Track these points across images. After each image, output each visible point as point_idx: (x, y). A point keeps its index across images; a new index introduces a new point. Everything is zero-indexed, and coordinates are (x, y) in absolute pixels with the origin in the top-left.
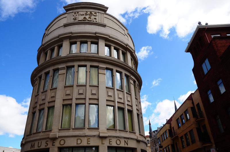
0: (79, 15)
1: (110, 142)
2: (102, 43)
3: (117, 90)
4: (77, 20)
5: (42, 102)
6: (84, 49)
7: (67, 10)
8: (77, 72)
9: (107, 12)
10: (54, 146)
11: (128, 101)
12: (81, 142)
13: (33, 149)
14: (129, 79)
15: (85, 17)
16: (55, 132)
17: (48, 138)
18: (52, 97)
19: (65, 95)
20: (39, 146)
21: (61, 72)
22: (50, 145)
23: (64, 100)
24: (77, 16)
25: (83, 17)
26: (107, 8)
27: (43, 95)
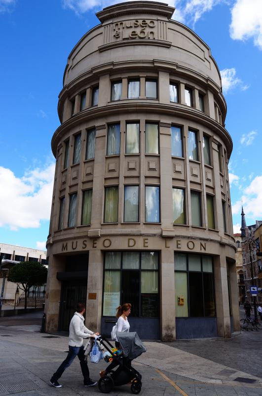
0: (124, 28)
1: (178, 244)
2: (164, 79)
3: (190, 161)
5: (73, 183)
10: (95, 249)
11: (208, 180)
12: (135, 244)
13: (65, 251)
15: (134, 32)
16: (95, 228)
17: (86, 236)
18: (88, 175)
21: (99, 133)
22: (89, 247)
23: (106, 179)
24: (121, 31)
25: (130, 31)
27: (74, 171)
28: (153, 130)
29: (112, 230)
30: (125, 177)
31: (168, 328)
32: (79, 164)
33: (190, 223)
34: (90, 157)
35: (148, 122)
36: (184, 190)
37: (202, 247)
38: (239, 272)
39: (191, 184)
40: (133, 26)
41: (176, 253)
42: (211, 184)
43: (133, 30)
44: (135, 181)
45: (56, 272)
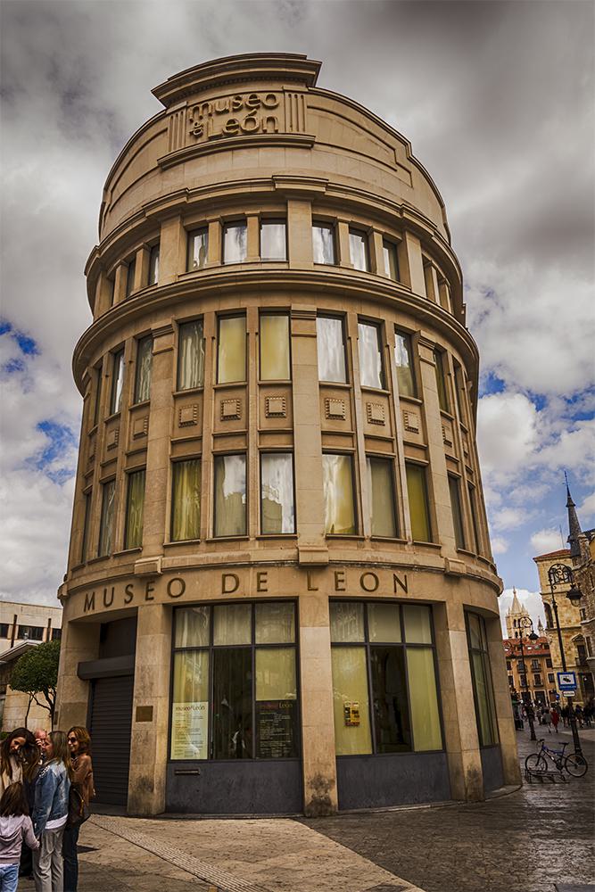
0: (210, 115)
1: (337, 581)
2: (299, 215)
3: (364, 391)
4: (204, 138)
5: (108, 457)
6: (236, 250)
7: (168, 102)
8: (257, 334)
9: (322, 83)
10: (152, 602)
11: (410, 429)
13: (90, 612)
14: (414, 343)
15: (232, 121)
16: (153, 556)
17: (132, 576)
18: (137, 436)
19: (176, 426)
20: (108, 602)
21: (159, 343)
22: (138, 600)
23: (174, 444)
24: (203, 122)
26: (316, 67)
27: (111, 432)
28: (277, 330)
29: (187, 557)
30: (216, 437)
31: (319, 783)
32: (119, 416)
33: (368, 532)
34: (143, 397)
35: (263, 312)
36: (350, 456)
37: (398, 585)
38: (575, 641)
39: (407, 447)
40: (231, 110)
41: (332, 600)
42: (419, 440)
43: (230, 116)
44: (237, 444)
45: (77, 661)
